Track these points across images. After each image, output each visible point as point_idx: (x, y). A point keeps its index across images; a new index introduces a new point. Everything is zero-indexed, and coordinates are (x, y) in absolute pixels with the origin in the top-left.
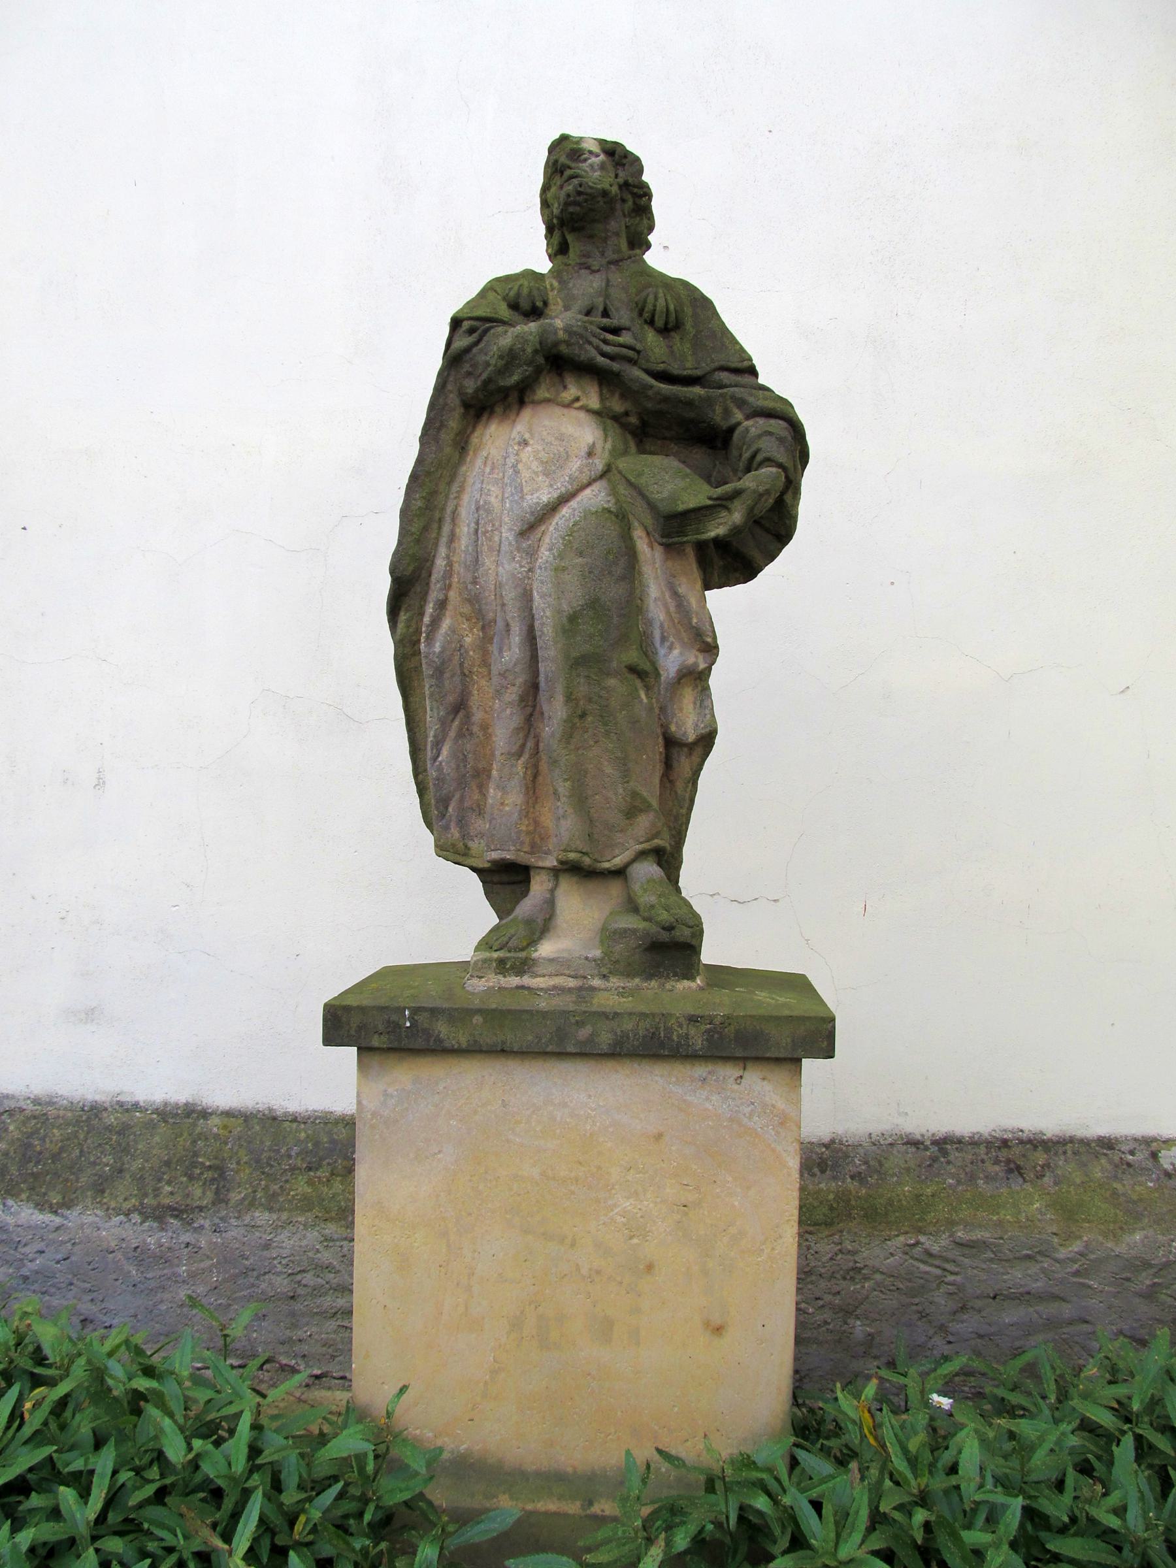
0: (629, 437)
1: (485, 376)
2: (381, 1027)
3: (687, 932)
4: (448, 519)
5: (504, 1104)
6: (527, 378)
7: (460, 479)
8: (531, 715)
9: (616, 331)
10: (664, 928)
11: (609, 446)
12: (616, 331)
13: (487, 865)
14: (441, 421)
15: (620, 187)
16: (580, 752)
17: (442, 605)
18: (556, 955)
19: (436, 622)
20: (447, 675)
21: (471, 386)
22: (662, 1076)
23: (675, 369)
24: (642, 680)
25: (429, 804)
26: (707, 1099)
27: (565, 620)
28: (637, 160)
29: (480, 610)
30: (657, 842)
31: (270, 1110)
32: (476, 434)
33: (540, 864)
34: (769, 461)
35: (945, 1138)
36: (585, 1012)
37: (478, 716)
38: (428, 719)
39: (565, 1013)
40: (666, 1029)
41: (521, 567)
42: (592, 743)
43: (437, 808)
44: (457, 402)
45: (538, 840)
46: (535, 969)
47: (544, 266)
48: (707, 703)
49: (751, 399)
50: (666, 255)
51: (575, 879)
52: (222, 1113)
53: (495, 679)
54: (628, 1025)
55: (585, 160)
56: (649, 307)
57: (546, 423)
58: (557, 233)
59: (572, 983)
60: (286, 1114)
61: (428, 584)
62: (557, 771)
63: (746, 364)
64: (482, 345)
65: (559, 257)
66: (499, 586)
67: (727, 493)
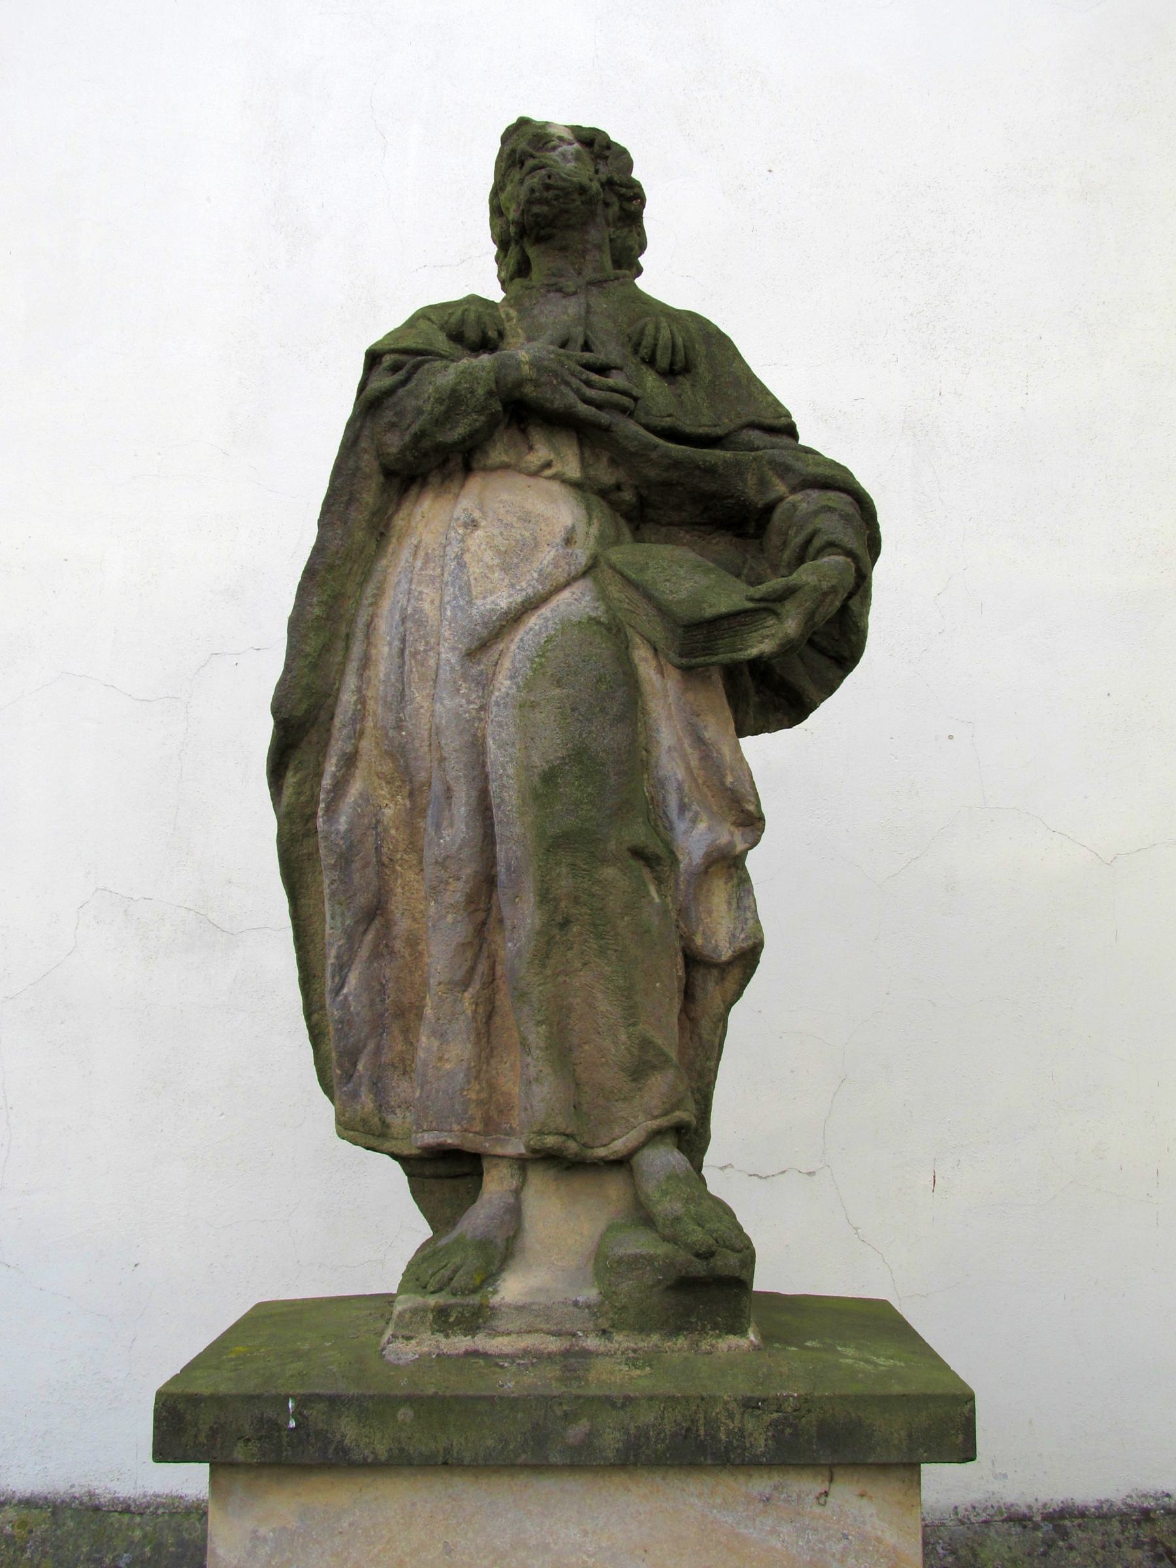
0: (622, 522)
1: (415, 428)
2: (248, 1430)
3: (733, 1259)
4: (359, 634)
5: (448, 1550)
6: (477, 431)
7: (377, 577)
8: (484, 923)
9: (603, 370)
10: (698, 1255)
11: (594, 530)
12: (603, 370)
13: (414, 1151)
14: (351, 493)
15: (602, 185)
16: (561, 979)
17: (350, 761)
18: (529, 1300)
19: (340, 786)
20: (357, 865)
21: (394, 443)
22: (700, 1495)
23: (688, 426)
24: (651, 868)
25: (327, 1058)
26: (773, 1531)
27: (536, 780)
28: (623, 152)
29: (407, 767)
30: (680, 1115)
31: (91, 1495)
32: (402, 514)
33: (499, 1151)
34: (832, 546)
35: (1062, 1510)
36: (578, 1397)
37: (402, 925)
38: (328, 931)
39: (546, 1401)
40: (708, 1421)
41: (469, 702)
42: (578, 965)
43: (341, 1066)
44: (375, 466)
45: (494, 1114)
46: (495, 1323)
47: (495, 293)
48: (746, 902)
49: (798, 465)
50: (664, 277)
51: (552, 1172)
52: (20, 1502)
53: (429, 871)
54: (647, 1417)
55: (554, 148)
56: (647, 341)
57: (505, 496)
58: (513, 250)
59: (554, 1345)
60: (114, 1501)
61: (328, 730)
62: (526, 1009)
63: (783, 420)
64: (411, 385)
65: (517, 280)
66: (436, 731)
67: (775, 591)
